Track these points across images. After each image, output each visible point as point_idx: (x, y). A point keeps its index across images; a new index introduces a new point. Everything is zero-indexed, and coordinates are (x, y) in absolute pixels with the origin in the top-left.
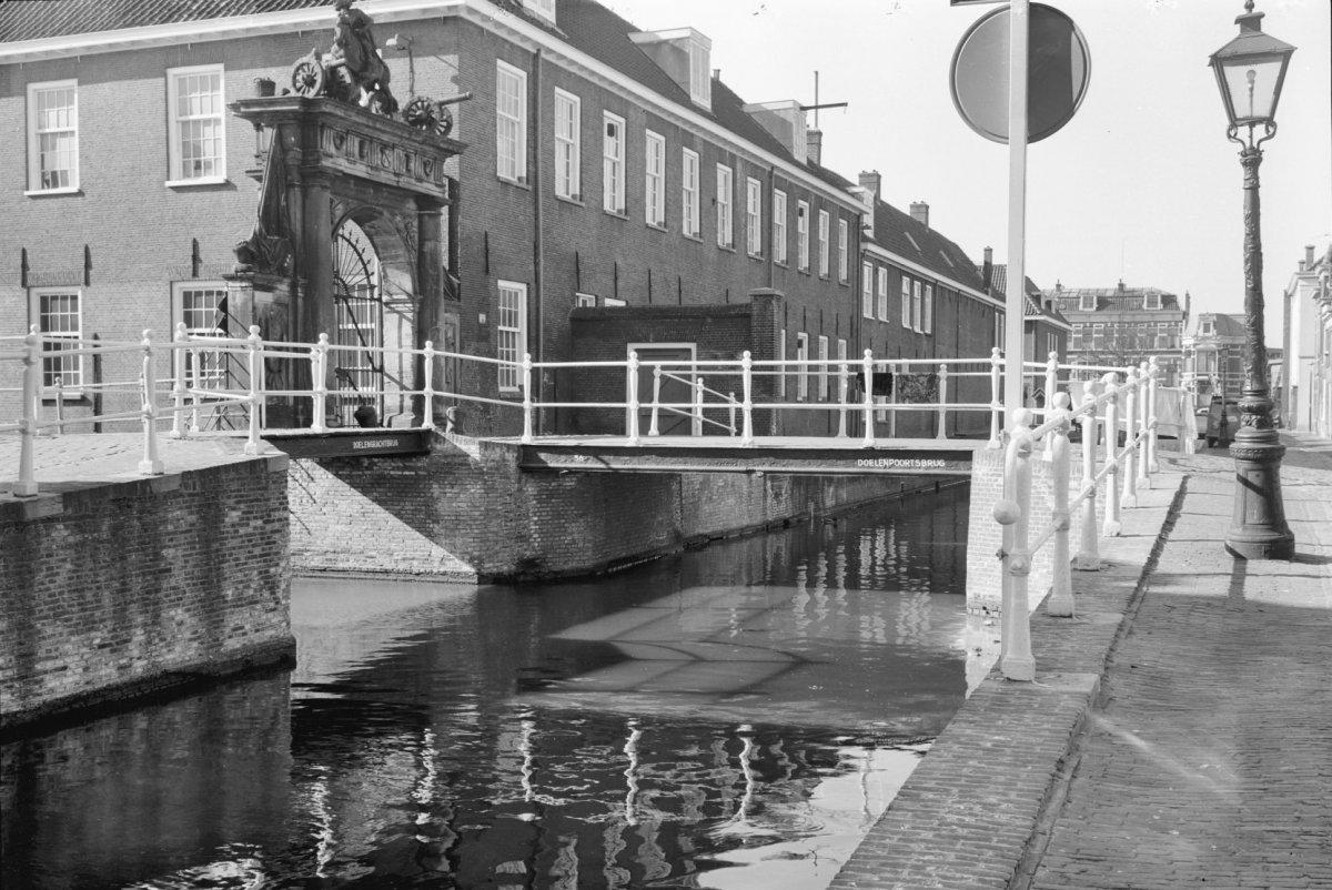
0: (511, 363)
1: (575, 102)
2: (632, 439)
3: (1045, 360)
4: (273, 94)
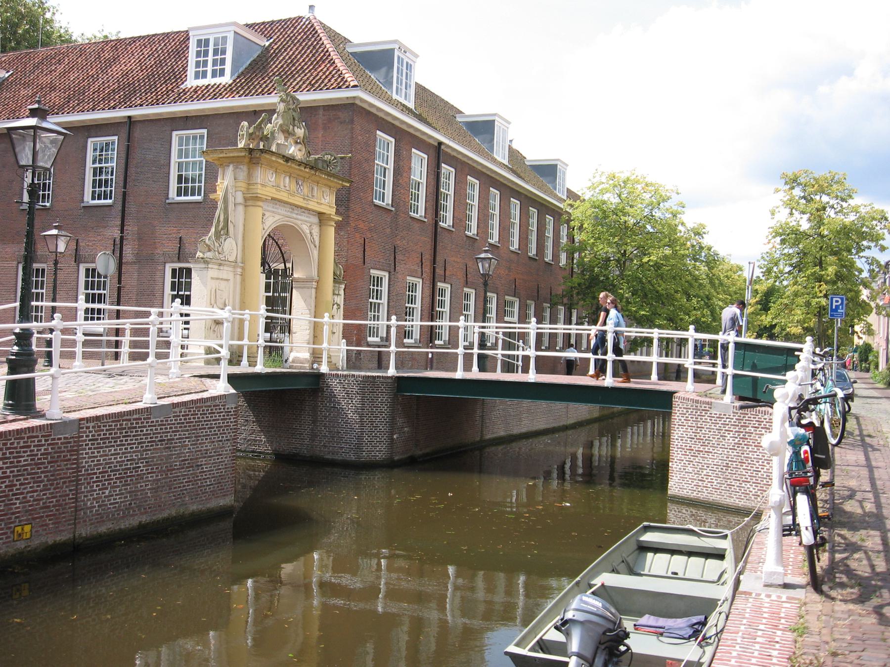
0: (376, 322)
1: (391, 142)
2: (459, 374)
3: (458, 321)
4: (650, 379)
